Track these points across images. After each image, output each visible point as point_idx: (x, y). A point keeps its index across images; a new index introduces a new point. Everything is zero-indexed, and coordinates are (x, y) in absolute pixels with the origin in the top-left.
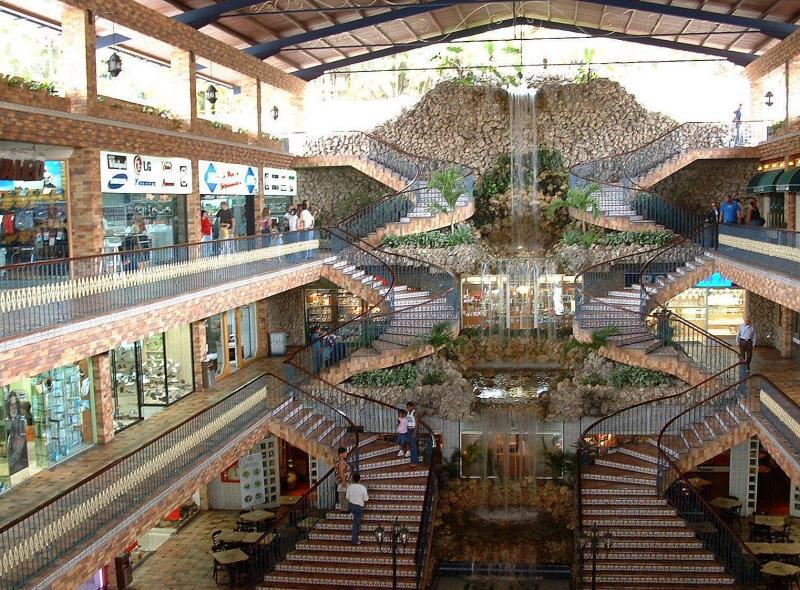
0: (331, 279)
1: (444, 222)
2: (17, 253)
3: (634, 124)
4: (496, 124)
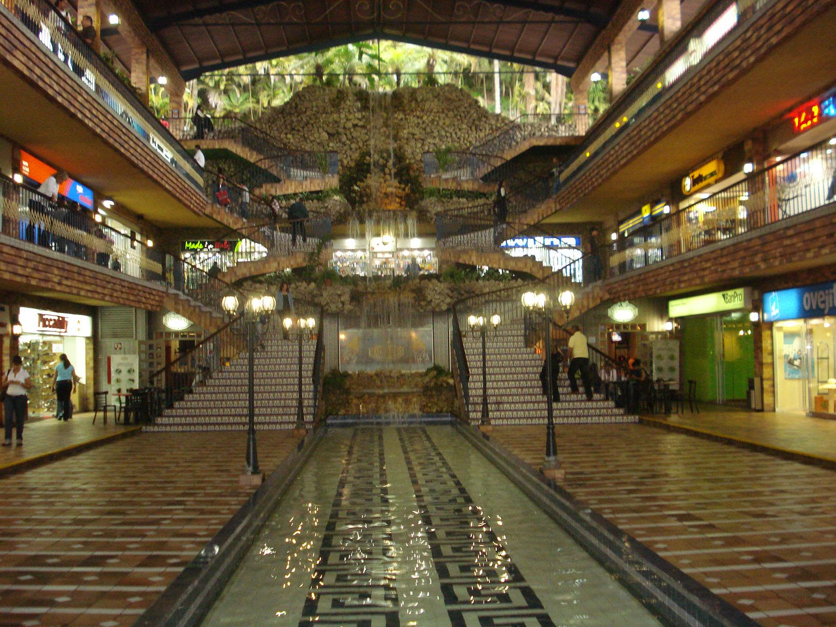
1: (314, 186)
2: (247, 468)
3: (477, 122)
4: (356, 122)
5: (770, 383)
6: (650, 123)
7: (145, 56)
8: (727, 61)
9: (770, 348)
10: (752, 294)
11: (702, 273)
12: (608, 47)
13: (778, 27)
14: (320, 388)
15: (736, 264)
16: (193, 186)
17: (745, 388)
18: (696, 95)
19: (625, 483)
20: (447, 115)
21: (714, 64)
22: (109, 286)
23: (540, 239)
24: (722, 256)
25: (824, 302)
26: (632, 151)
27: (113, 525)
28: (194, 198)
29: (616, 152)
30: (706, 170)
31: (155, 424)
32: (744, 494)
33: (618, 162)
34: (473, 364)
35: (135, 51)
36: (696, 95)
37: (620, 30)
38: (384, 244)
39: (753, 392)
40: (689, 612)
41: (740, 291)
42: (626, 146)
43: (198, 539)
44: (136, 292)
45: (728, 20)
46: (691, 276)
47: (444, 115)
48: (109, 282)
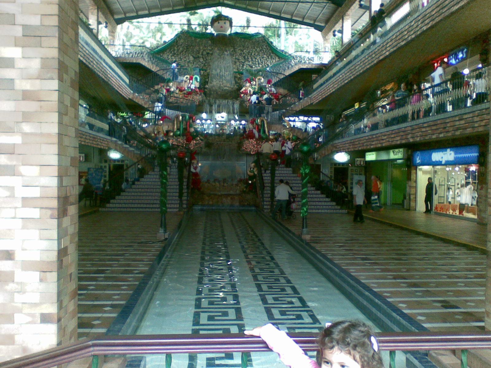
0: (134, 100)
4: (208, 51)
5: (414, 196)
6: (361, 63)
7: (96, 11)
8: (401, 36)
9: (415, 179)
10: (407, 152)
11: (382, 142)
12: (342, 17)
13: (427, 21)
14: (190, 191)
15: (398, 138)
16: (124, 84)
17: (402, 198)
18: (384, 52)
19: (338, 243)
20: (256, 50)
21: (394, 37)
22: (84, 137)
23: (302, 118)
24: (392, 134)
25: (442, 158)
26: (351, 77)
27: (102, 256)
28: (124, 90)
29: (343, 76)
30: (389, 87)
31: (106, 207)
32: (394, 250)
33: (344, 82)
34: (266, 181)
35: (91, 7)
36: (384, 52)
37: (349, 8)
38: (223, 117)
39: (405, 201)
40: (358, 294)
41: (401, 150)
42: (348, 74)
43: (145, 263)
44: (96, 140)
45: (405, 9)
46: (376, 142)
47: (254, 50)
48: (84, 135)
